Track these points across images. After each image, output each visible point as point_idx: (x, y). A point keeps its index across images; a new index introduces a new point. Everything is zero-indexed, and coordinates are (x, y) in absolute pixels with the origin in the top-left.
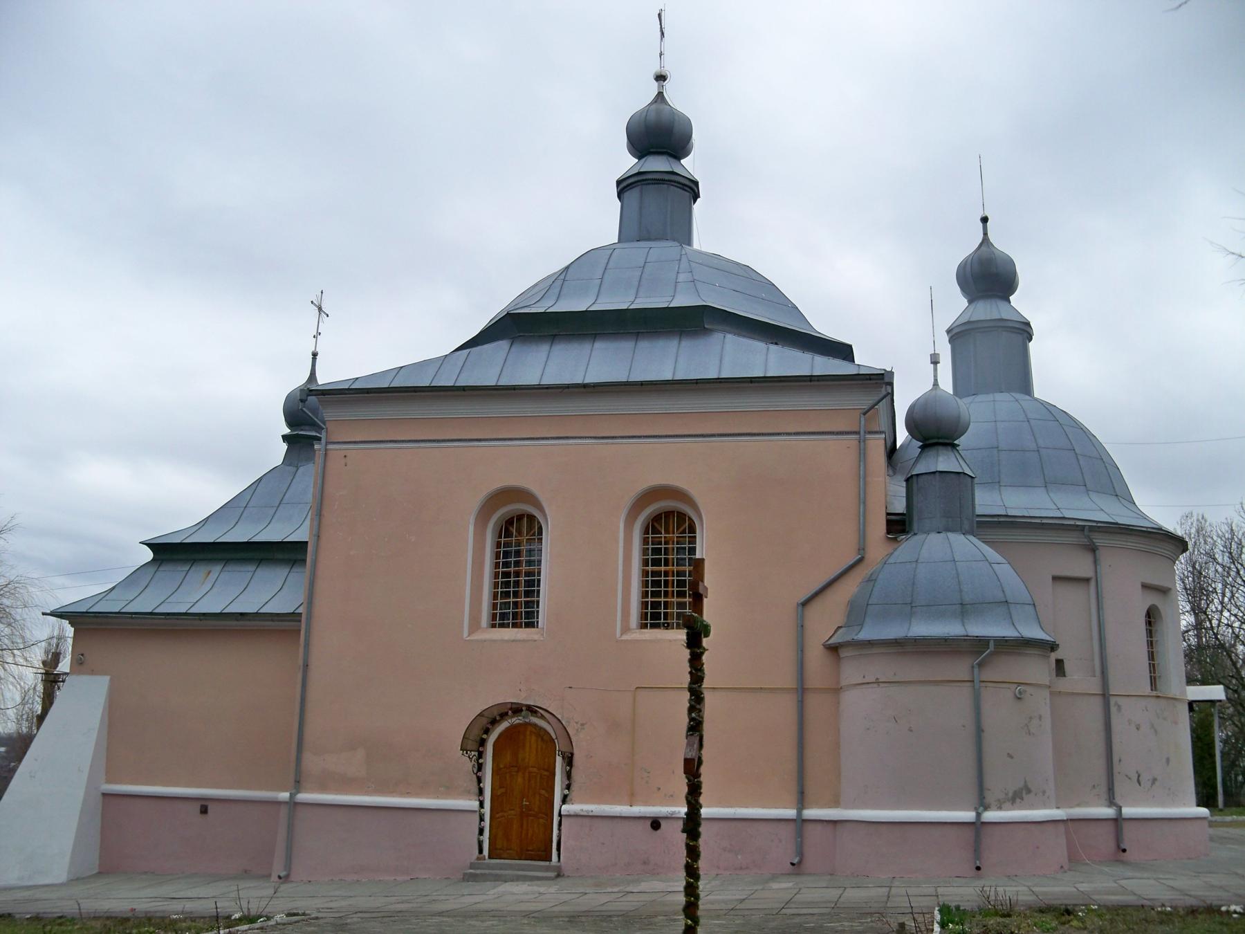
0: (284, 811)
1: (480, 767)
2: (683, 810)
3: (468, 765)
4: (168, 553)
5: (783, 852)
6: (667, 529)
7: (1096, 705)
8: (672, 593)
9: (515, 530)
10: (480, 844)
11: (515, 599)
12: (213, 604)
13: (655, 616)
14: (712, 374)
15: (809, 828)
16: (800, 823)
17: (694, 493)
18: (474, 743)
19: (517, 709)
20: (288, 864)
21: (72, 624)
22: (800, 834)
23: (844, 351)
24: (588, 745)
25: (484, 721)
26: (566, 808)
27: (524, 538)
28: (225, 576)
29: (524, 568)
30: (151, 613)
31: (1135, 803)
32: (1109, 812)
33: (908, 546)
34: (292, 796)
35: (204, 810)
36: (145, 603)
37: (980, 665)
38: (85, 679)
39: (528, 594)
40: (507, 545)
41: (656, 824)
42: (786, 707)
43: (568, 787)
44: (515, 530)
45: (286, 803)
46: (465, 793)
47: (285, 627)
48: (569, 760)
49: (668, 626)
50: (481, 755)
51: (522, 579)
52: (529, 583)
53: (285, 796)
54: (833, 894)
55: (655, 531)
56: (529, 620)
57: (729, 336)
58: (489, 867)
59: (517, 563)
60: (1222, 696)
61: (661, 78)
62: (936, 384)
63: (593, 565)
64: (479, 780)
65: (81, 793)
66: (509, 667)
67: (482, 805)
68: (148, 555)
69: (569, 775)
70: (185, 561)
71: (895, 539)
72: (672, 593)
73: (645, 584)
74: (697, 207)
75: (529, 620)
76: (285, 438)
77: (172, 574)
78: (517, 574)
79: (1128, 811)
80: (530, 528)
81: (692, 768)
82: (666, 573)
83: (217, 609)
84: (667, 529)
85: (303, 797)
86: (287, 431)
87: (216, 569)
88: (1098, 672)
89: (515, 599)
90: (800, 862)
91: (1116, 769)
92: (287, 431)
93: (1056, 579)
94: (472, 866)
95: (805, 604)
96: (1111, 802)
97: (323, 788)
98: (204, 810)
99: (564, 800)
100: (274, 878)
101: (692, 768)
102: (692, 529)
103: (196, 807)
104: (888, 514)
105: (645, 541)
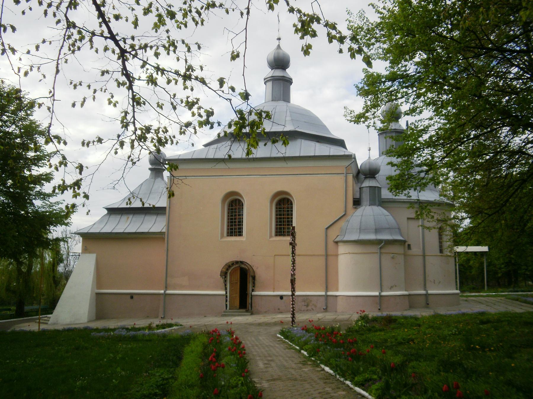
0: (162, 297)
1: (225, 281)
2: (290, 293)
3: (222, 280)
4: (112, 211)
5: (321, 304)
6: (283, 205)
7: (421, 259)
8: (284, 223)
9: (234, 206)
10: (226, 305)
11: (235, 226)
12: (132, 229)
13: (232, 232)
14: (297, 155)
15: (329, 297)
16: (327, 296)
17: (292, 193)
18: (224, 274)
19: (237, 262)
20: (164, 314)
21: (81, 236)
22: (326, 300)
23: (341, 143)
24: (261, 273)
25: (227, 267)
26: (254, 293)
27: (237, 207)
28: (134, 219)
29: (237, 217)
30: (123, 233)
31: (431, 290)
32: (423, 292)
33: (360, 211)
34: (165, 292)
35: (132, 297)
36: (108, 229)
37: (381, 248)
38: (87, 255)
39: (239, 225)
40: (232, 209)
41: (281, 297)
42: (322, 260)
43: (254, 286)
44: (234, 206)
45: (162, 294)
46: (221, 289)
47: (158, 237)
48: (254, 278)
49: (284, 235)
50: (225, 277)
51: (237, 220)
52: (239, 222)
53: (162, 292)
54: (334, 317)
55: (280, 205)
56: (240, 233)
57: (303, 141)
58: (230, 312)
59: (235, 215)
60: (47, 262)
61: (279, 39)
62: (369, 157)
63: (258, 215)
64: (226, 285)
65: (89, 293)
66: (236, 249)
67: (226, 293)
68: (106, 212)
69: (254, 283)
70: (119, 214)
71: (355, 208)
72: (284, 223)
73: (277, 222)
74: (292, 87)
75: (240, 233)
76: (150, 169)
77: (115, 219)
78: (235, 219)
79: (430, 292)
80: (239, 204)
81: (293, 282)
82: (283, 218)
83: (134, 231)
84: (283, 205)
85: (168, 292)
86: (150, 166)
87: (131, 216)
88: (421, 247)
89: (235, 226)
90: (326, 309)
91: (427, 278)
92: (150, 166)
93: (408, 219)
94: (224, 312)
95: (327, 228)
96: (425, 290)
97: (175, 289)
98: (132, 297)
99: (253, 290)
100: (160, 317)
101: (293, 282)
102: (292, 204)
103: (129, 296)
104: (354, 199)
105: (277, 208)
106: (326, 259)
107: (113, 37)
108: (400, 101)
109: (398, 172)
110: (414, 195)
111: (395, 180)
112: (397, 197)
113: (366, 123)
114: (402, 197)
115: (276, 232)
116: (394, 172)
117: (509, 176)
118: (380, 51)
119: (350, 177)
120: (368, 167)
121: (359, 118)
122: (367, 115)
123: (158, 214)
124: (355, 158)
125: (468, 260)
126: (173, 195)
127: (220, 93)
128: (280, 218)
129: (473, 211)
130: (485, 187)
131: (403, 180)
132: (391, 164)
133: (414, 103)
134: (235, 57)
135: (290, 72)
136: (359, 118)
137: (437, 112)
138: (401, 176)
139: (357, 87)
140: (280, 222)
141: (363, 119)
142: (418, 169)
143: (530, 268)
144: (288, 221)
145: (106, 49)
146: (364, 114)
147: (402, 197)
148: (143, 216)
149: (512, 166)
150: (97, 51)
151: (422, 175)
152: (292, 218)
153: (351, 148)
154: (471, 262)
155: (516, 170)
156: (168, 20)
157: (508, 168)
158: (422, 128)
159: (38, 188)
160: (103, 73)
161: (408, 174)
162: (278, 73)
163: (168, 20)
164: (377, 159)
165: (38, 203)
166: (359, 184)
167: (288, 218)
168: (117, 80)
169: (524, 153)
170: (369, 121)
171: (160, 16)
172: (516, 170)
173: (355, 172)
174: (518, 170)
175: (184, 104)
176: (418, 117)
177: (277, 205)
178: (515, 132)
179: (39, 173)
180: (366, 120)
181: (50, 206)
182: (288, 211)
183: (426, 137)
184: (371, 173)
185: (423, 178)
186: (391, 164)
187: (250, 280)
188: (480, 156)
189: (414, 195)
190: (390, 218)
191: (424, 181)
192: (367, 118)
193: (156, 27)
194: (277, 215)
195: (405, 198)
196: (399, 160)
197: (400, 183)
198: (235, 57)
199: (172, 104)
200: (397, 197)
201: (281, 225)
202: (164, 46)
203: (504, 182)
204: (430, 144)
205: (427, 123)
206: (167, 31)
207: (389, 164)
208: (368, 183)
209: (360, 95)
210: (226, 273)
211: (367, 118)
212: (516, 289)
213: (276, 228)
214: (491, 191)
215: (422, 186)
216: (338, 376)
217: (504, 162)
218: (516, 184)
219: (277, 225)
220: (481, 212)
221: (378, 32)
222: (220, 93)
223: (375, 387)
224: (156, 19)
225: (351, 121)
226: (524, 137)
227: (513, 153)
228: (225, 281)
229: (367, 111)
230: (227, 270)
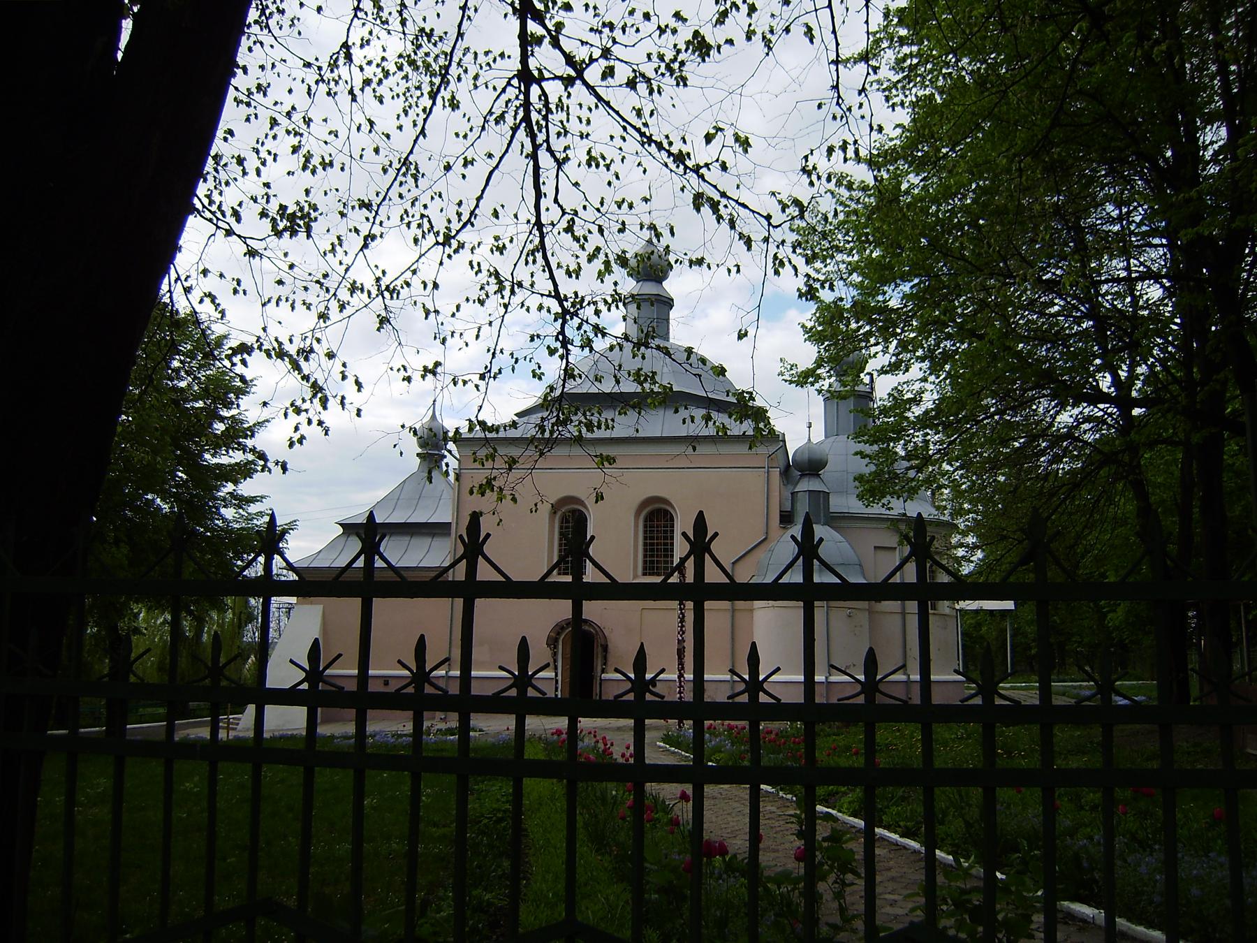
1: (555, 654)
48: (605, 648)
68: (341, 530)
73: (645, 550)
92: (419, 451)
99: (603, 671)
102: (672, 519)
105: (645, 526)
106: (733, 617)
107: (557, 295)
108: (873, 350)
109: (873, 468)
110: (897, 507)
111: (868, 482)
112: (869, 510)
113: (817, 386)
114: (876, 509)
115: (645, 568)
116: (866, 468)
117: (1051, 478)
118: (842, 267)
119: (776, 473)
120: (806, 457)
121: (805, 378)
122: (819, 371)
123: (433, 535)
124: (784, 441)
125: (978, 625)
126: (602, 498)
127: (688, 367)
128: (652, 544)
129: (988, 535)
130: (1011, 493)
131: (880, 481)
132: (862, 455)
133: (896, 355)
134: (742, 335)
135: (672, 286)
136: (805, 378)
137: (935, 369)
138: (878, 474)
139: (803, 326)
140: (652, 550)
141: (811, 379)
142: (906, 464)
143: (1086, 640)
144: (666, 550)
145: (540, 308)
146: (814, 370)
147: (876, 509)
148: (407, 538)
149: (1057, 459)
150: (528, 310)
151: (912, 474)
152: (672, 544)
153: (778, 422)
154: (984, 629)
155: (1064, 466)
156: (615, 267)
157: (1050, 462)
158: (909, 395)
159: (230, 487)
160: (532, 339)
161: (889, 473)
162: (649, 288)
163: (615, 267)
164: (822, 442)
165: (229, 513)
166: (790, 487)
167: (666, 544)
168: (548, 347)
169: (1077, 439)
170: (821, 382)
171: (607, 263)
172: (1064, 466)
173: (782, 464)
174: (1067, 468)
175: (631, 378)
176: (901, 377)
177: (645, 521)
178: (1062, 406)
179: (233, 461)
180: (816, 381)
181: (247, 519)
182: (666, 532)
183: (917, 411)
184: (812, 466)
185: (913, 479)
186: (862, 455)
187: (598, 651)
188: (1005, 443)
189: (897, 507)
190: (845, 546)
191: (914, 484)
192: (819, 377)
193: (601, 276)
194: (645, 538)
195: (883, 511)
196: (875, 447)
197: (876, 486)
198: (742, 335)
199: (615, 376)
200: (869, 510)
201: (652, 556)
202: (606, 302)
203: (1042, 487)
204: (925, 422)
205: (917, 386)
206: (616, 284)
207: (856, 454)
208: (806, 485)
209: (809, 339)
210: (556, 640)
211: (819, 377)
212: (1061, 677)
213: (645, 562)
214: (1023, 501)
215: (911, 492)
216: (781, 794)
217: (1043, 452)
218: (1064, 489)
219: (645, 556)
220: (1004, 538)
221: (840, 236)
222: (688, 367)
223: (847, 799)
224: (602, 267)
225: (791, 382)
226: (1076, 411)
227: (1057, 439)
228: (555, 654)
229: (819, 367)
230: (559, 634)
